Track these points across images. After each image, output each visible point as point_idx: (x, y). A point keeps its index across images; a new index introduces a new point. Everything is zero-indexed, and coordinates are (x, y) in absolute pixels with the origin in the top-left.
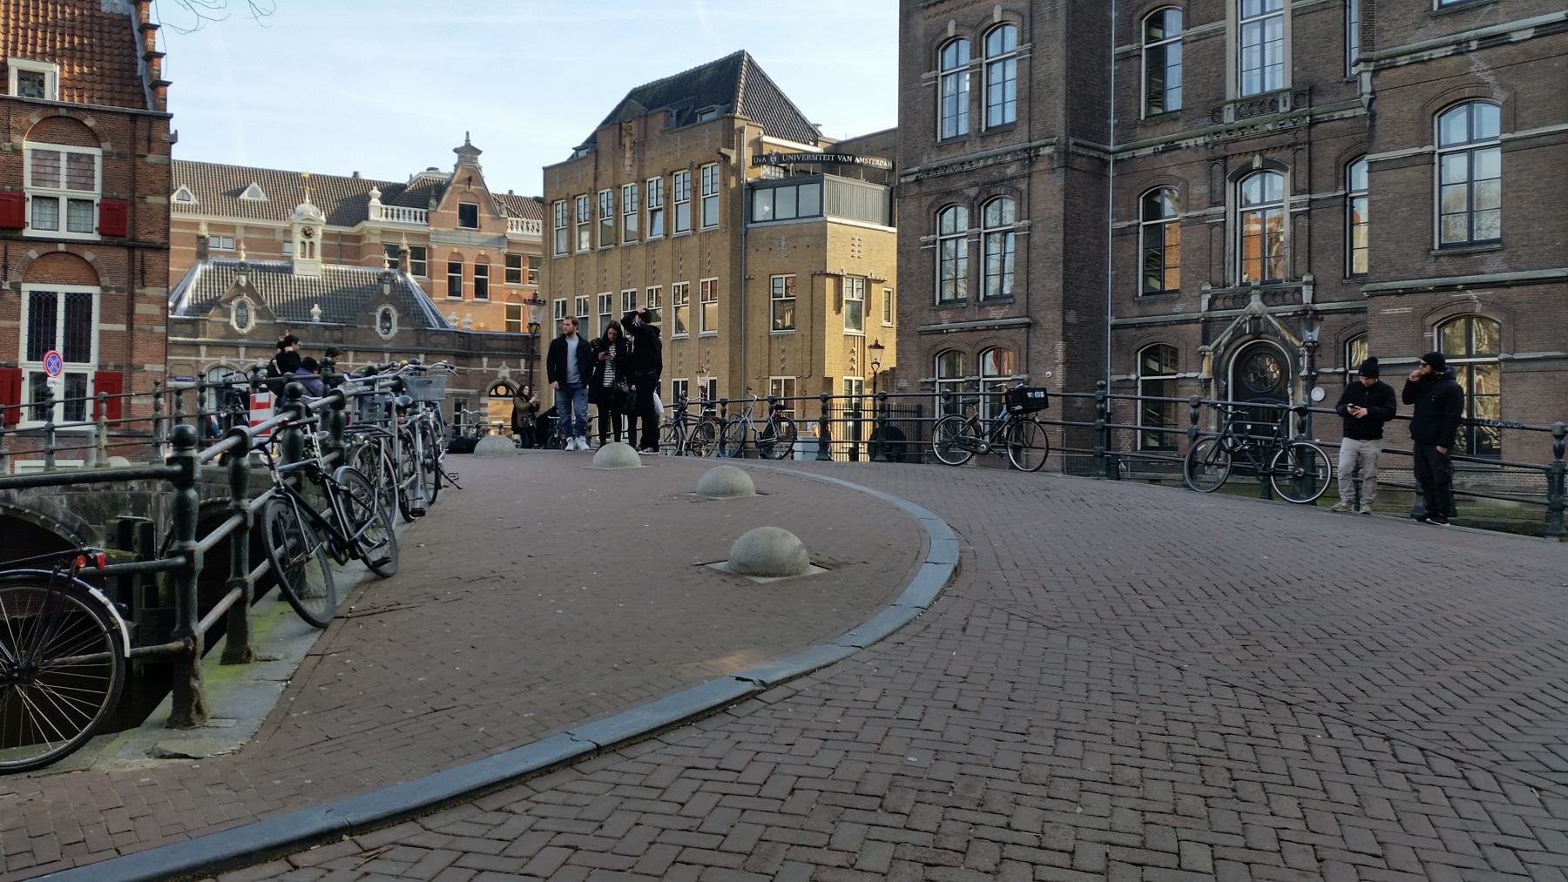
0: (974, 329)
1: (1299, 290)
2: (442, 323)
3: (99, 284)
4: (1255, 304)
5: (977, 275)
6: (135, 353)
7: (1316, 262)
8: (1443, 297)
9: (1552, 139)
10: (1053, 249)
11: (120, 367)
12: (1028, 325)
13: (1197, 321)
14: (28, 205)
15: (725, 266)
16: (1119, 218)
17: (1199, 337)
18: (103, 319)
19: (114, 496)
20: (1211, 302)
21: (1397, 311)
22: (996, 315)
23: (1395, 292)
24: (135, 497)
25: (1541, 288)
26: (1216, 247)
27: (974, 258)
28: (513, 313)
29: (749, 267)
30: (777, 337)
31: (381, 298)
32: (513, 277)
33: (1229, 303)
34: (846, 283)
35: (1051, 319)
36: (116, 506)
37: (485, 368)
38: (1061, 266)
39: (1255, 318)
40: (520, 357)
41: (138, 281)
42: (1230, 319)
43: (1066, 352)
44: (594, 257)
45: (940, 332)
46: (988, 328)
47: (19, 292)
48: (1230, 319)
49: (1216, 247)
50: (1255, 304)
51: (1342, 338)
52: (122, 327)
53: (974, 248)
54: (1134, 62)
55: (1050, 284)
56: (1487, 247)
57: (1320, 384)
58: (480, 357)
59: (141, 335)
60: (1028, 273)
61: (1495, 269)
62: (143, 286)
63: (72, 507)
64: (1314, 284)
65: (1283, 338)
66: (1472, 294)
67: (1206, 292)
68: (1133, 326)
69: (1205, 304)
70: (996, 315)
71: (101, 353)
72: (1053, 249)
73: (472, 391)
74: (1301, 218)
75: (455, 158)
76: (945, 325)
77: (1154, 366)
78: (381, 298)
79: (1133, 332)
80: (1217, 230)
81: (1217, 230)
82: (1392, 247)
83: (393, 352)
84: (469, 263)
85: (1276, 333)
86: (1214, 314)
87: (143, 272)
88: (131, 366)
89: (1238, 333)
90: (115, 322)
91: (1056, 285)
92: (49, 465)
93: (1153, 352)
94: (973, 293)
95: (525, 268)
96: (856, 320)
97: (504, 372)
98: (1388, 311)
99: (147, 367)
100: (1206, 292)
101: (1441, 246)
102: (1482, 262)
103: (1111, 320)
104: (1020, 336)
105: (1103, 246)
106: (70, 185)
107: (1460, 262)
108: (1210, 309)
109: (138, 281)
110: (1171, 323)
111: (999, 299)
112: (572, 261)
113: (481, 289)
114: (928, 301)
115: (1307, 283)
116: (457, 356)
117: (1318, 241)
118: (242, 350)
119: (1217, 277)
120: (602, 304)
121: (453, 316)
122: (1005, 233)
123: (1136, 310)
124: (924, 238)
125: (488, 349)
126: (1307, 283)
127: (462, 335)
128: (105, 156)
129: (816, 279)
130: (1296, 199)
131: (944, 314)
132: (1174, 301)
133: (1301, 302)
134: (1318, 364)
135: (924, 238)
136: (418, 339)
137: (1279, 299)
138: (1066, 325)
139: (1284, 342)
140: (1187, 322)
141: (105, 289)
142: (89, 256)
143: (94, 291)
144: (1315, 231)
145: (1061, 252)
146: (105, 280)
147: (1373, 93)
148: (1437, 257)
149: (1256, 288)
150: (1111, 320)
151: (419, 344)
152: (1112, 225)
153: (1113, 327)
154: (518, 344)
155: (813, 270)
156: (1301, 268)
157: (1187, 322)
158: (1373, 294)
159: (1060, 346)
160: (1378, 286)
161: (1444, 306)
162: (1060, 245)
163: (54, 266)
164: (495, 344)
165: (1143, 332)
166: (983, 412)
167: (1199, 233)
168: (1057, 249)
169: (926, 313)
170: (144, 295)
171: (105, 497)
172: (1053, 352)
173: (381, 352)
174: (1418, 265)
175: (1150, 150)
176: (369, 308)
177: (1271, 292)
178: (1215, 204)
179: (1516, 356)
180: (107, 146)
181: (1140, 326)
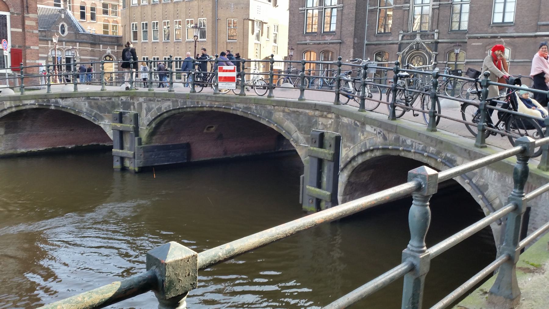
0: (319, 44)
1: (433, 35)
2: (84, 31)
3: (9, 11)
4: (418, 38)
5: (321, 24)
6: (27, 41)
7: (440, 25)
8: (493, 40)
10: (351, 16)
11: (21, 47)
12: (340, 43)
13: (397, 44)
15: (210, 14)
16: (371, 5)
17: (397, 49)
18: (12, 26)
19: (113, 102)
20: (402, 37)
21: (477, 44)
22: (328, 39)
23: (477, 38)
24: (124, 103)
25: (525, 39)
26: (405, 18)
27: (320, 17)
28: (106, 27)
29: (219, 15)
30: (230, 43)
31: (61, 20)
32: (105, 12)
33: (409, 38)
34: (255, 23)
35: (349, 41)
36: (114, 106)
37: (101, 49)
38: (354, 22)
39: (418, 43)
40: (115, 45)
41: (26, 11)
42: (409, 43)
43: (354, 53)
44: (150, 7)
45: (306, 44)
46: (325, 43)
48: (409, 43)
49: (405, 18)
50: (418, 38)
51: (446, 52)
52: (20, 30)
53: (320, 13)
55: (350, 28)
56: (509, 24)
57: (438, 66)
58: (99, 44)
59: (28, 34)
60: (341, 24)
61: (511, 32)
62: (28, 13)
63: (91, 106)
64: (439, 33)
65: (427, 51)
66: (502, 40)
67: (401, 34)
68: (374, 44)
69: (400, 38)
70: (328, 39)
71: (12, 41)
72: (351, 16)
73: (96, 58)
74: (436, 10)
76: (308, 41)
77: (380, 59)
78: (61, 20)
79: (373, 46)
80: (406, 12)
81: (406, 12)
82: (477, 22)
83: (66, 42)
84: (88, 7)
85: (424, 49)
86: (403, 41)
87: (27, 7)
88: (25, 46)
89: (411, 48)
90: (18, 28)
91: (352, 29)
92: (76, 89)
93: (379, 54)
94: (319, 30)
95: (110, 9)
96: (258, 37)
97: (109, 51)
98: (474, 44)
99: (32, 47)
100: (401, 34)
101: (493, 23)
102: (507, 29)
103: (366, 42)
104: (337, 47)
105: (365, 15)
107: (500, 28)
108: (402, 39)
109: (26, 11)
110: (387, 44)
111: (330, 33)
112: (140, 8)
113: (93, 17)
114: (301, 32)
115: (437, 32)
116: (91, 44)
117: (441, 18)
118: (64, 43)
119: (405, 29)
120: (154, 26)
121: (89, 28)
122: (332, 8)
123: (375, 39)
124: (301, 9)
125: (102, 41)
126: (437, 32)
127: (92, 35)
129: (245, 21)
130: (435, 3)
131: (307, 38)
132: (389, 36)
133: (434, 39)
134: (437, 60)
135: (301, 9)
136: (76, 37)
137: (426, 37)
138: (354, 43)
139: (427, 52)
140: (393, 44)
141: (12, 13)
143: (8, 14)
144: (440, 15)
145: (354, 17)
146: (12, 10)
148: (492, 27)
149: (418, 33)
150: (366, 42)
151: (76, 39)
152: (368, 8)
153: (366, 45)
154: (114, 40)
155: (244, 17)
156: (435, 27)
157: (393, 44)
158: (470, 38)
159: (352, 51)
160: (472, 35)
161: (493, 43)
162: (354, 14)
164: (105, 39)
165: (377, 47)
166: (174, 69)
167: (400, 12)
168: (353, 15)
169: (300, 37)
170: (29, 17)
171: (108, 103)
172: (349, 53)
174: (485, 29)
176: (55, 23)
177: (424, 35)
178: (406, 3)
179: (515, 60)
181: (376, 45)
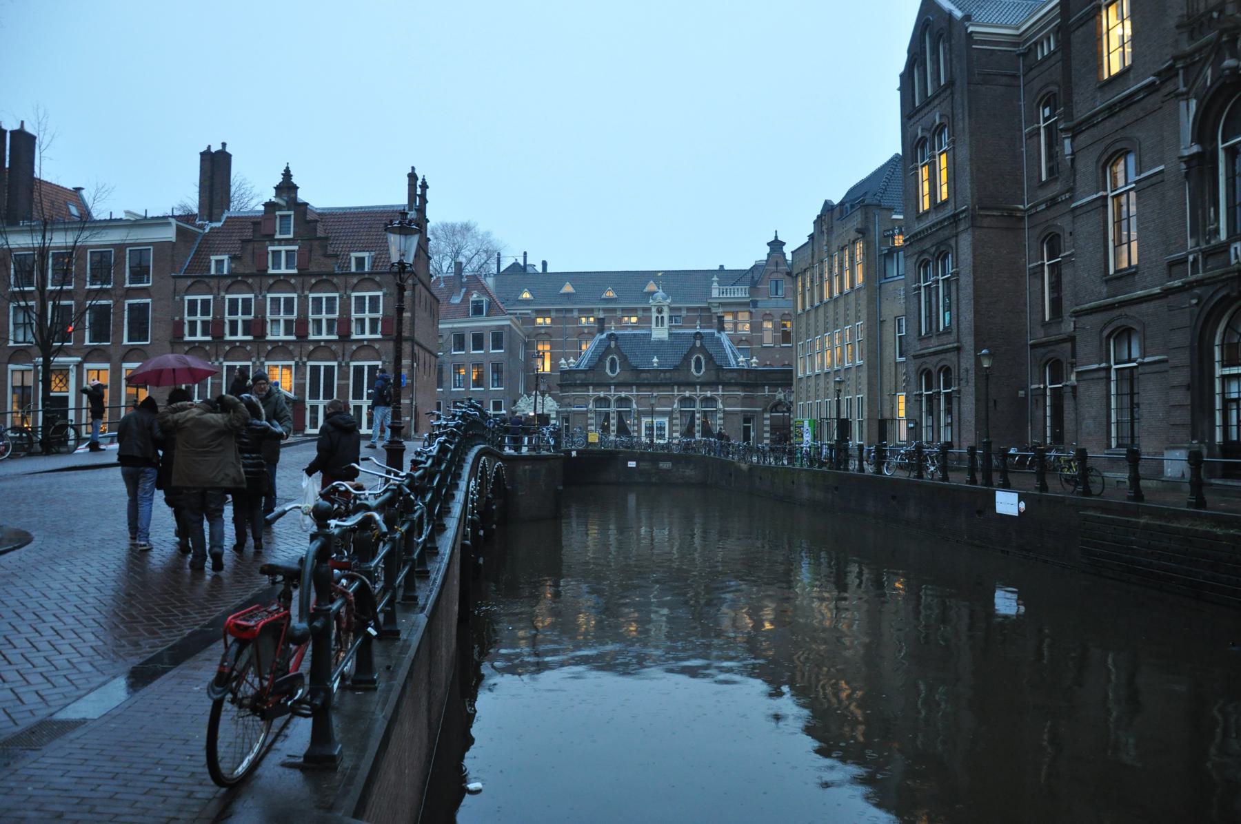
9: (1148, 182)
14: (269, 326)
47: (349, 367)
54: (1035, 139)
58: (764, 386)
75: (768, 249)
106: (244, 321)
128: (384, 295)
142: (334, 347)
146: (384, 358)
147: (1073, 153)
163: (363, 353)
173: (608, 385)
175: (1043, 206)
180: (385, 290)
